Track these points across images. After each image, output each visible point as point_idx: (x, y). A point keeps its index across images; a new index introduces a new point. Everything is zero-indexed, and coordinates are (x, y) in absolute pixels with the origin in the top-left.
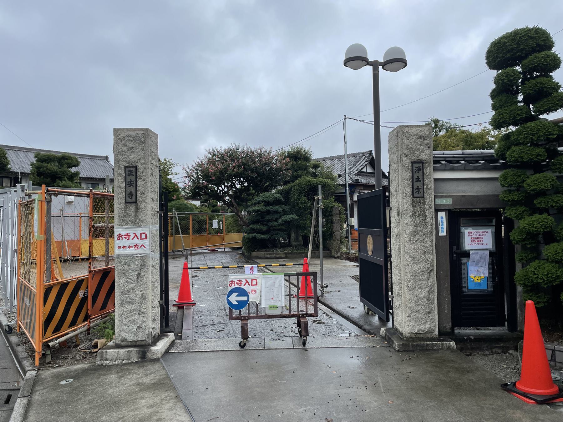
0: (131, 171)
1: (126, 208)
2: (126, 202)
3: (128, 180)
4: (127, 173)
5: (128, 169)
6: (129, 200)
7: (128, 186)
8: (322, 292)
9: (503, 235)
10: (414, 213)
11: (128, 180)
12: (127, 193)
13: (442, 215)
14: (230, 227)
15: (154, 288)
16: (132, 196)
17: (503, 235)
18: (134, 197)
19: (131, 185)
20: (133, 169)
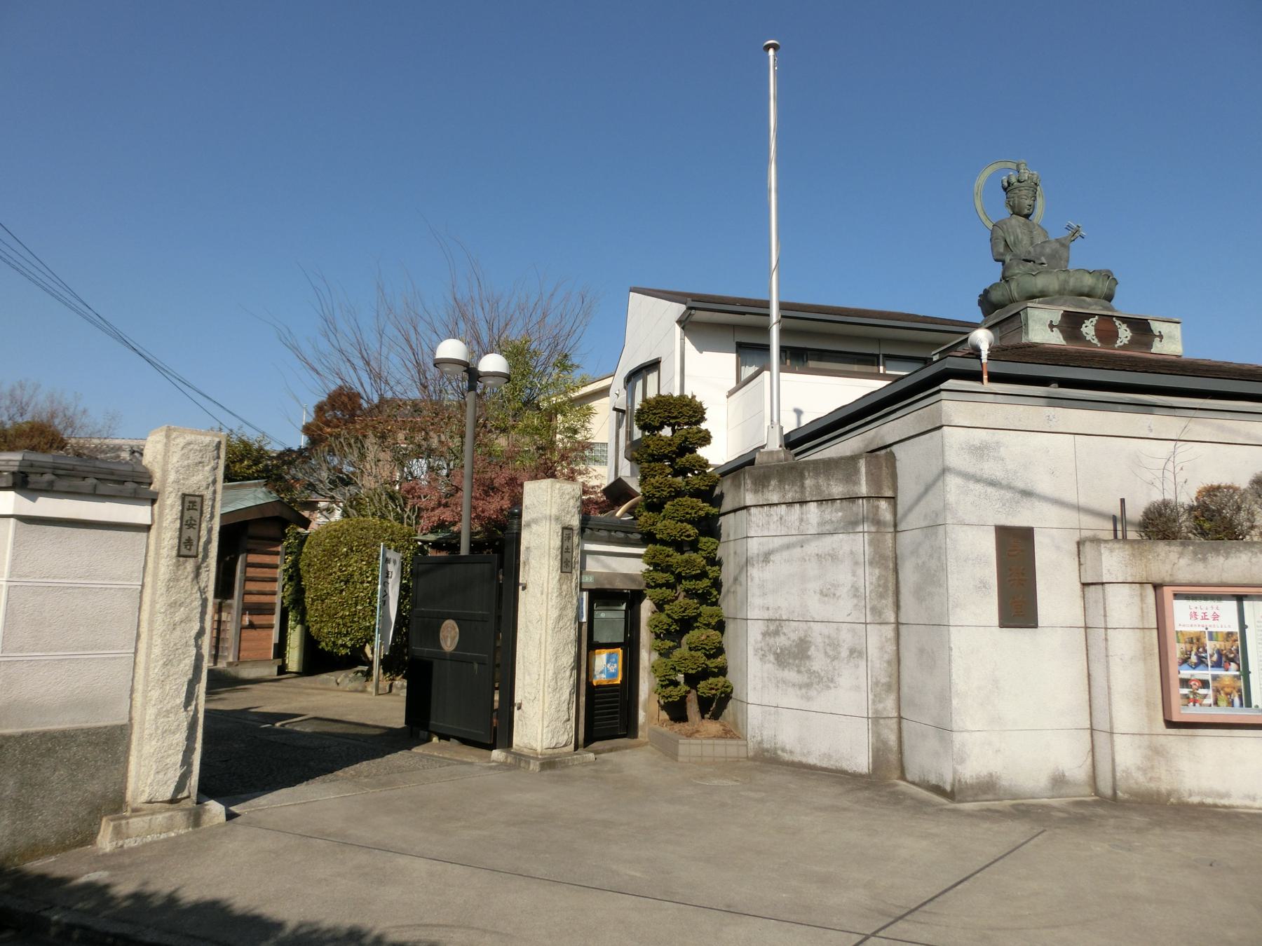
0: (193, 503)
1: (178, 565)
2: (179, 555)
3: (186, 517)
4: (187, 505)
5: (188, 499)
6: (184, 551)
7: (185, 527)
8: (672, 573)
9: (496, 705)
10: (560, 594)
11: (186, 517)
12: (183, 540)
13: (585, 595)
14: (1207, 525)
15: (453, 639)
16: (191, 545)
17: (496, 705)
18: (194, 548)
19: (190, 526)
20: (198, 499)
